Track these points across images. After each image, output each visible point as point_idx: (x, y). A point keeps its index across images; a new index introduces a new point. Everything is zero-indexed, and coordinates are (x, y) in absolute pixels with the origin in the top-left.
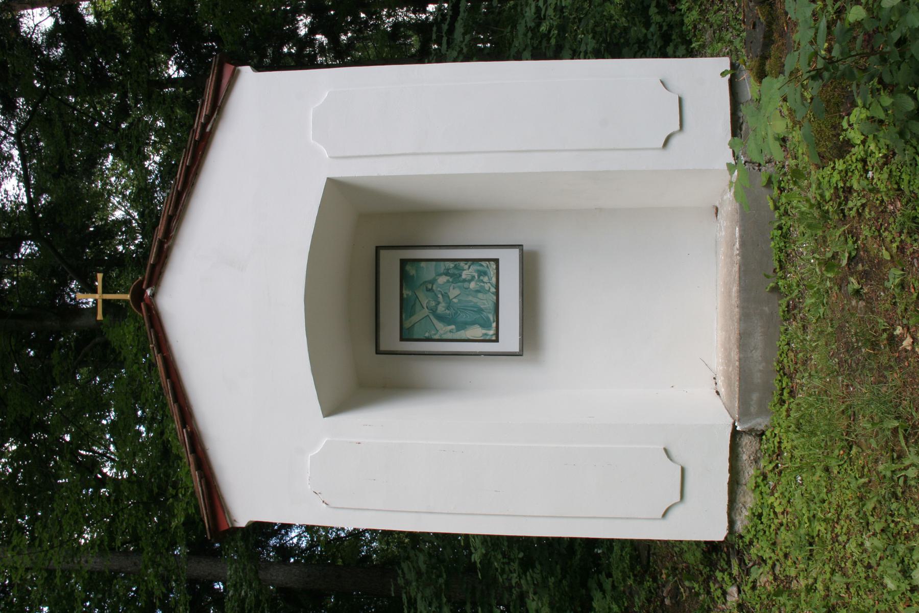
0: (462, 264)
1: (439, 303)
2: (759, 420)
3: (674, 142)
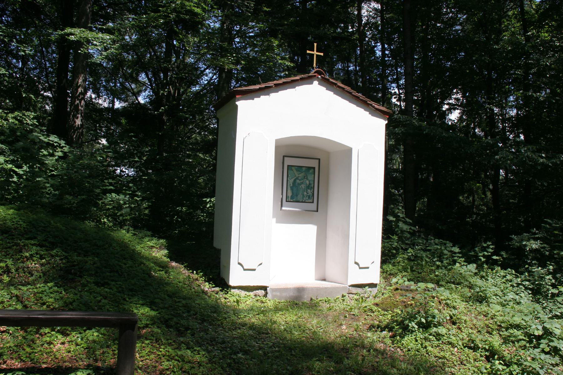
0: (312, 190)
1: (300, 180)
2: (270, 296)
3: (357, 266)
